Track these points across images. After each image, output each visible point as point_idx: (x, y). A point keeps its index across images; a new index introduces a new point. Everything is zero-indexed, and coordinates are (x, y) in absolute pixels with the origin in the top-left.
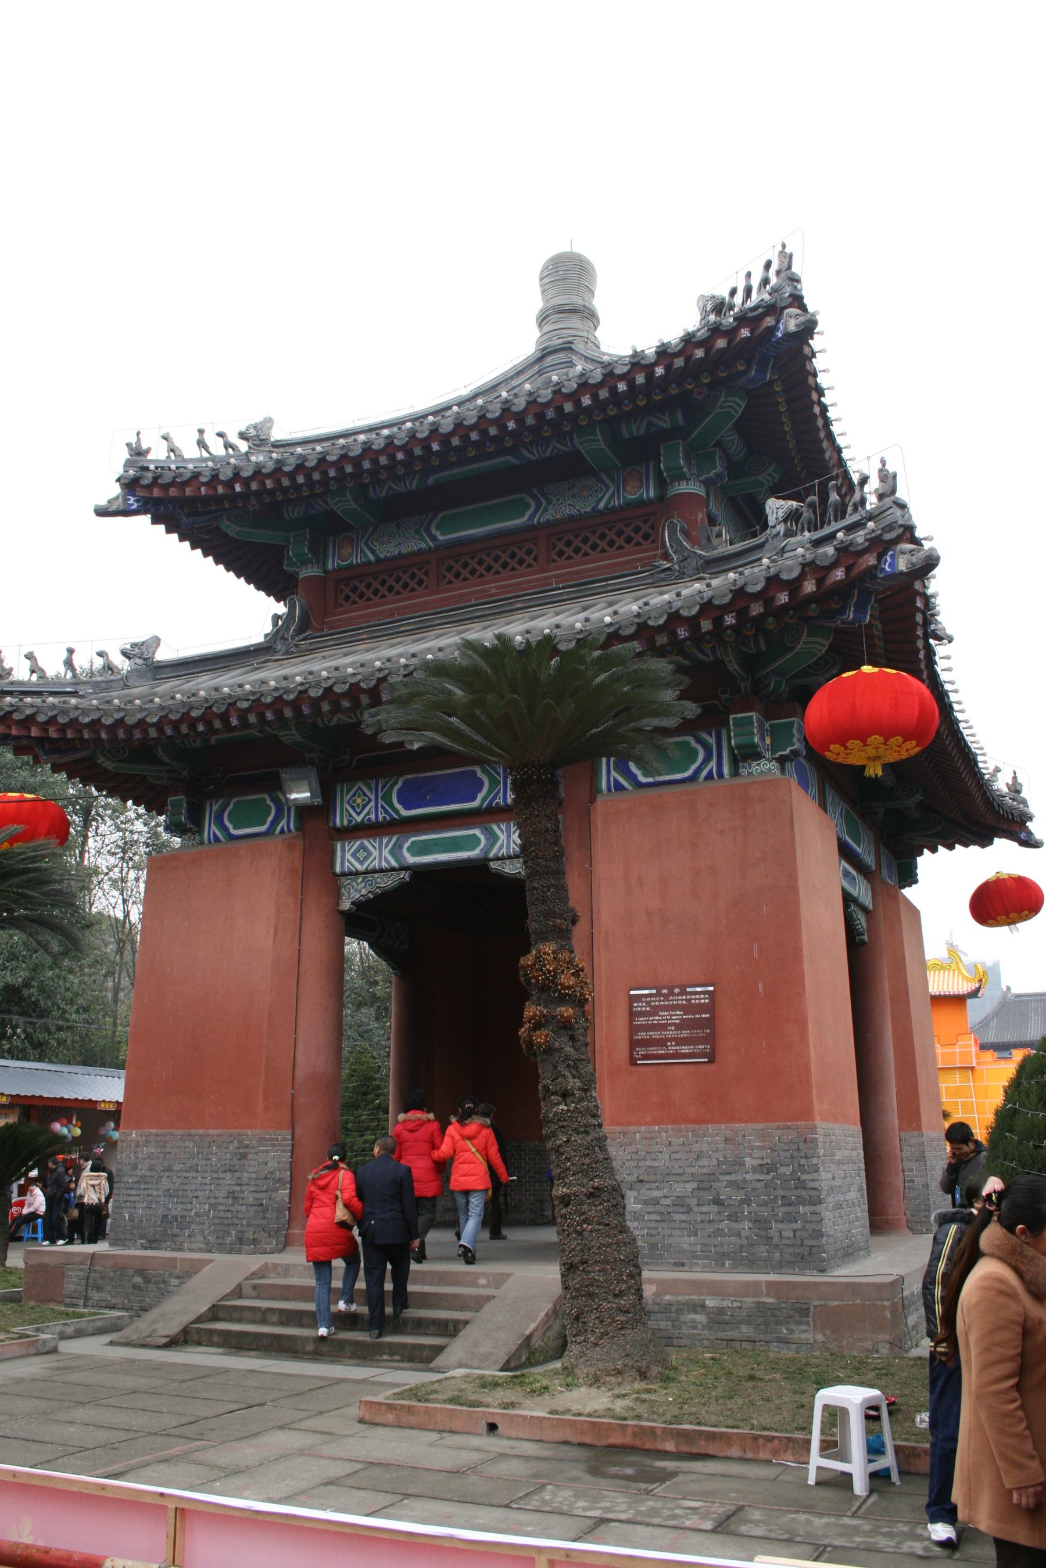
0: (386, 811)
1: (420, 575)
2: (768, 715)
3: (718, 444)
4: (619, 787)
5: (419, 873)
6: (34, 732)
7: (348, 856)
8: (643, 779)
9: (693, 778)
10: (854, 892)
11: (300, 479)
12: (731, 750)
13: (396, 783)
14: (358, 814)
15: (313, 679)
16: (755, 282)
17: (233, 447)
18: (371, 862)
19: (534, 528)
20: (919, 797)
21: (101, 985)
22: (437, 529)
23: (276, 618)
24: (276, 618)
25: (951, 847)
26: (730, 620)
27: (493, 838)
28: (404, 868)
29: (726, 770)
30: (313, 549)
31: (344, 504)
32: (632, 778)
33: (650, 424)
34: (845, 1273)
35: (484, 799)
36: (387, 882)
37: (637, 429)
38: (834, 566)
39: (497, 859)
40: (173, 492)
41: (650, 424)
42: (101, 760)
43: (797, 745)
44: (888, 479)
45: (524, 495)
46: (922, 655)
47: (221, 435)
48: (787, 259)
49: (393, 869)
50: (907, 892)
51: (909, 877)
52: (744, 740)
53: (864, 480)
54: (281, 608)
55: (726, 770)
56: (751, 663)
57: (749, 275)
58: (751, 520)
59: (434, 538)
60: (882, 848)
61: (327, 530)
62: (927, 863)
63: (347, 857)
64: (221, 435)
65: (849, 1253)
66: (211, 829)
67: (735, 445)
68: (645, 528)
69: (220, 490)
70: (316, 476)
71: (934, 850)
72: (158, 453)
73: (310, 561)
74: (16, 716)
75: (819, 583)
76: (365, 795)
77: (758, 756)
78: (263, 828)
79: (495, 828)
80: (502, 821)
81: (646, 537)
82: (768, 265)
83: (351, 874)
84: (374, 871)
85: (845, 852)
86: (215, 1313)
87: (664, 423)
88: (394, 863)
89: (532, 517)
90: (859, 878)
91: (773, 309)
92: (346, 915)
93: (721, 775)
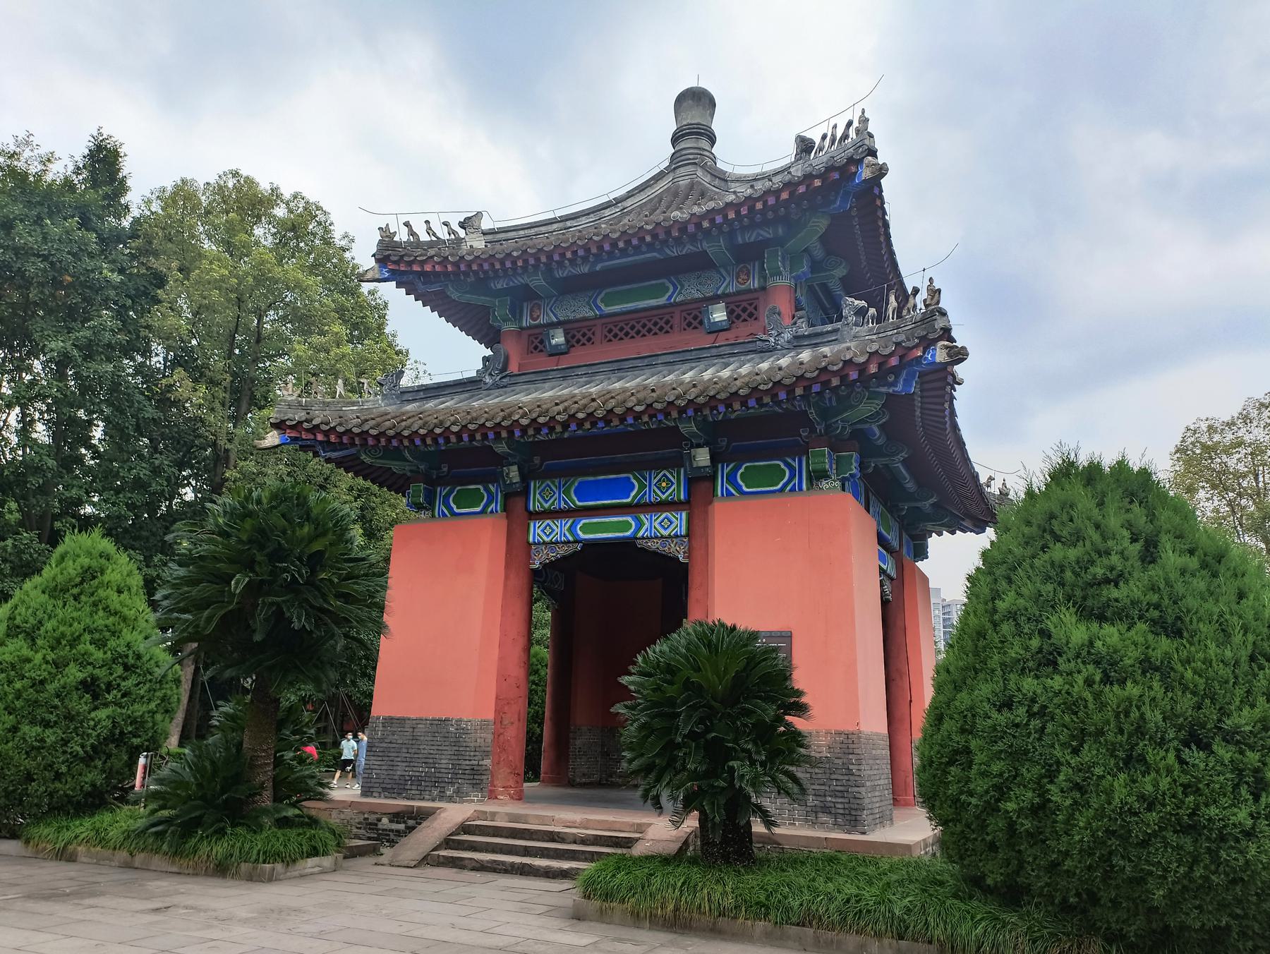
0: (566, 503)
1: (589, 334)
2: (833, 449)
3: (806, 250)
4: (729, 494)
5: (590, 545)
6: (320, 437)
7: (538, 531)
8: (745, 489)
9: (782, 490)
10: (885, 567)
11: (508, 264)
12: (808, 472)
13: (573, 483)
14: (547, 502)
15: (507, 411)
16: (839, 134)
17: (454, 232)
18: (552, 535)
19: (672, 305)
20: (933, 500)
21: (21, 359)
22: (602, 301)
23: (485, 359)
24: (485, 359)
25: (953, 533)
26: (816, 388)
27: (640, 525)
28: (576, 542)
29: (804, 487)
30: (513, 312)
31: (537, 281)
32: (738, 488)
33: (759, 234)
34: (878, 835)
35: (635, 497)
36: (562, 551)
37: (751, 237)
38: (891, 354)
39: (643, 538)
40: (416, 268)
41: (759, 234)
42: (363, 457)
43: (854, 471)
44: (935, 293)
45: (665, 281)
46: (947, 413)
47: (446, 224)
48: (864, 121)
49: (569, 542)
50: (920, 564)
51: (921, 553)
52: (819, 467)
53: (916, 291)
54: (489, 352)
55: (804, 487)
56: (825, 414)
57: (835, 127)
58: (832, 312)
59: (599, 308)
60: (872, 498)
61: (524, 297)
62: (935, 543)
63: (537, 531)
64: (446, 224)
65: (884, 819)
66: (439, 507)
67: (819, 253)
68: (750, 309)
69: (450, 268)
70: (520, 263)
71: (940, 534)
72: (402, 236)
73: (510, 320)
74: (305, 425)
75: (880, 365)
76: (669, 480)
77: (827, 477)
78: (478, 509)
79: (642, 517)
80: (647, 512)
81: (751, 315)
82: (850, 124)
83: (539, 543)
84: (557, 542)
85: (882, 541)
86: (448, 843)
87: (767, 234)
88: (571, 539)
89: (670, 298)
90: (888, 556)
91: (855, 161)
92: (535, 572)
93: (801, 489)
